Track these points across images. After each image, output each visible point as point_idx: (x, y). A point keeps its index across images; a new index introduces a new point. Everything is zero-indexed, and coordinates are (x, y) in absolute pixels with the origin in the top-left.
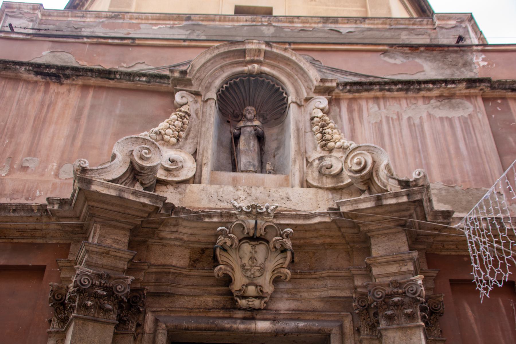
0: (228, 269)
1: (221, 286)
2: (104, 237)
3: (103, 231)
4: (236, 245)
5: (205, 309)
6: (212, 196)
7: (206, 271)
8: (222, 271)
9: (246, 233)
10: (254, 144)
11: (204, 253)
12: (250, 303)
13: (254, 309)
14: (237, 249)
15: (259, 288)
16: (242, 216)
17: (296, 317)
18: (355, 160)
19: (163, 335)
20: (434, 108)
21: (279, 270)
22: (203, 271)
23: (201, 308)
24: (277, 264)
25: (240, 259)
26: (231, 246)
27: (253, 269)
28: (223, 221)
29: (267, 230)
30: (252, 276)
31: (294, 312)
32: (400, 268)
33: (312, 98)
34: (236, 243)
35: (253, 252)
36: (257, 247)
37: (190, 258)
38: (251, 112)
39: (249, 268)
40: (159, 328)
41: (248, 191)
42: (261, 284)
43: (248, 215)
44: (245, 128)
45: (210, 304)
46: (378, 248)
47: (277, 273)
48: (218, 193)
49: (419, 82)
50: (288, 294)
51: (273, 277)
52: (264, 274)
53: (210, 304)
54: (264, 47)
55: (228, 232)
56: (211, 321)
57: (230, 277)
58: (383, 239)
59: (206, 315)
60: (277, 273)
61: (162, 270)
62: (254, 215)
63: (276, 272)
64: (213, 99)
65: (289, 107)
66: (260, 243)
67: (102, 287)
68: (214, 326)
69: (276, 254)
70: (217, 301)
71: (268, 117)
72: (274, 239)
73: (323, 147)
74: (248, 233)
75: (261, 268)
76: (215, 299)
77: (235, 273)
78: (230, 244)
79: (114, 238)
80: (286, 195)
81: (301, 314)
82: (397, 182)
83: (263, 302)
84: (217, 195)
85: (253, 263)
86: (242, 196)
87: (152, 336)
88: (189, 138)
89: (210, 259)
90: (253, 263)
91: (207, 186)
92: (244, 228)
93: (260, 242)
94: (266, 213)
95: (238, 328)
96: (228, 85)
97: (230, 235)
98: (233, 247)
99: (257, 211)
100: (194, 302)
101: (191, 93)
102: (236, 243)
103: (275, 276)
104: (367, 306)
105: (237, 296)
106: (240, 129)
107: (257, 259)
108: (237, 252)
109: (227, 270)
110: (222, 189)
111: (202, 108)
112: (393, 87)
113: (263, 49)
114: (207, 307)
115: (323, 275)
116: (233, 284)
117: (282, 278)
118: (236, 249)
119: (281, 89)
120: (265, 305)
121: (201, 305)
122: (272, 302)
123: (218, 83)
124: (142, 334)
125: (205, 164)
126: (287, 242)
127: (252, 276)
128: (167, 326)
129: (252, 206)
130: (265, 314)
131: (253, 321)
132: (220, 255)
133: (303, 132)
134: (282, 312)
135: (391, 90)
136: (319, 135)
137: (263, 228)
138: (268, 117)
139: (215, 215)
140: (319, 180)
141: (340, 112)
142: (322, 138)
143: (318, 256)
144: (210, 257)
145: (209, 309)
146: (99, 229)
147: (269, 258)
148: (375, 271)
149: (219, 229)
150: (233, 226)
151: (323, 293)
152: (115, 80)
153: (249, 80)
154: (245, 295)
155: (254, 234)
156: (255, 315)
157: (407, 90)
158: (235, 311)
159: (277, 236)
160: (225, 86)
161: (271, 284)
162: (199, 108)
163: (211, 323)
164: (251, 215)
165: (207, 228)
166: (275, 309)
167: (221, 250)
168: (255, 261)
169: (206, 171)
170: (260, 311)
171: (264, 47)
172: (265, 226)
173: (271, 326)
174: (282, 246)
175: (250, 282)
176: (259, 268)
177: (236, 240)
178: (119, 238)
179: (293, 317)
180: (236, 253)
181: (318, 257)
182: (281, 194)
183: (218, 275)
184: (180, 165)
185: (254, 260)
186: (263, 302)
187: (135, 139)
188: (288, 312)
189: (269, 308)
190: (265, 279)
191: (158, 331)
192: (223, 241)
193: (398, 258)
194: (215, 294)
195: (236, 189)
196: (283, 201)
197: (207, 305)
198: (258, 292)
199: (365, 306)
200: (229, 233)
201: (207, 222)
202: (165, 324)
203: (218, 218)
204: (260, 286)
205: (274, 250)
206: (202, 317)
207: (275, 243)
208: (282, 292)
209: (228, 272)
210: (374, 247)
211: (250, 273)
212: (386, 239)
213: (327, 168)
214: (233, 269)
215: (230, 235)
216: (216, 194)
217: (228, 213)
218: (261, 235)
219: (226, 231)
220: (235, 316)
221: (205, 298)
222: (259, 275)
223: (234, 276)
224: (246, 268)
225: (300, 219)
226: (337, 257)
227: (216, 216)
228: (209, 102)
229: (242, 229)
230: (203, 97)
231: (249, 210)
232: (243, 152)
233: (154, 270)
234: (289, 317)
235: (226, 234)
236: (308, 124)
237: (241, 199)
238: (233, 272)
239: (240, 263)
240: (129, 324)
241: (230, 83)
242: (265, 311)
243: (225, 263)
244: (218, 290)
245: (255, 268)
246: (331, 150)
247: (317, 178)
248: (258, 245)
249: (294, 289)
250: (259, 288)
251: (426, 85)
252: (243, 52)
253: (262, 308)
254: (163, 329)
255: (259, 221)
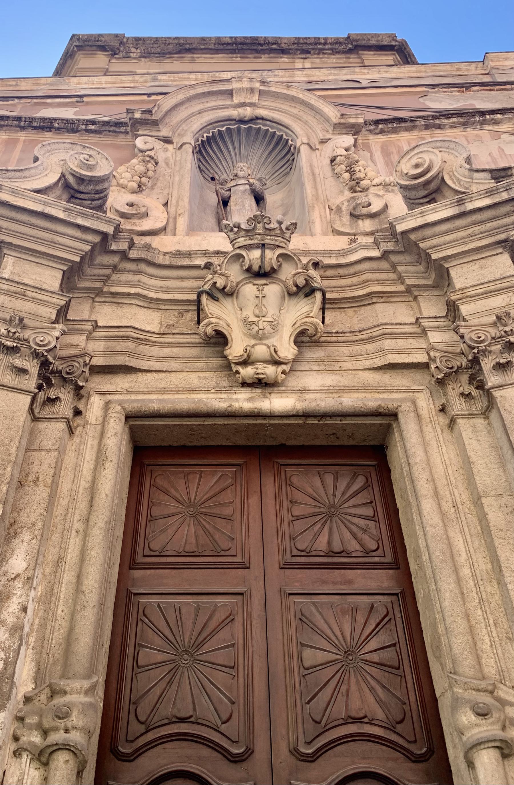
2: (20, 276)
3: (17, 268)
10: (251, 205)
18: (414, 161)
19: (117, 421)
20: (507, 143)
24: (299, 313)
32: (509, 299)
33: (330, 139)
37: (160, 323)
38: (244, 168)
40: (110, 411)
44: (237, 187)
45: (194, 382)
46: (466, 281)
49: (482, 113)
54: (257, 85)
58: (472, 268)
61: (116, 333)
64: (190, 144)
65: (299, 152)
67: (10, 337)
70: (205, 378)
71: (267, 182)
73: (353, 190)
76: (202, 376)
77: (232, 331)
79: (36, 279)
82: (487, 175)
87: (99, 427)
88: (156, 187)
89: (192, 324)
96: (211, 135)
100: (168, 380)
101: (159, 139)
104: (456, 368)
106: (230, 190)
111: (174, 156)
112: (445, 121)
113: (257, 88)
115: (375, 334)
117: (309, 332)
119: (284, 137)
123: (197, 124)
124: (84, 426)
125: (180, 215)
128: (124, 409)
133: (322, 177)
135: (442, 126)
136: (347, 176)
138: (267, 182)
140: (351, 225)
141: (371, 156)
142: (351, 178)
143: (361, 315)
144: (193, 321)
146: (11, 264)
148: (465, 309)
151: (376, 361)
152: (53, 130)
153: (239, 129)
155: (260, 267)
157: (465, 125)
160: (205, 135)
161: (292, 344)
162: (170, 156)
168: (264, 309)
169: (182, 223)
171: (257, 85)
178: (44, 280)
181: (362, 316)
184: (143, 210)
185: (263, 307)
187: (71, 146)
191: (108, 416)
193: (503, 285)
199: (452, 368)
202: (120, 404)
207: (295, 278)
209: (221, 329)
210: (457, 281)
212: (477, 266)
213: (363, 207)
226: (394, 313)
228: (184, 147)
230: (175, 144)
232: (236, 212)
233: (103, 334)
234: (42, 668)
236: (328, 168)
238: (229, 329)
240: (60, 406)
241: (213, 132)
246: (365, 190)
247: (348, 223)
248: (267, 284)
251: (492, 116)
252: (230, 93)
254: (117, 412)
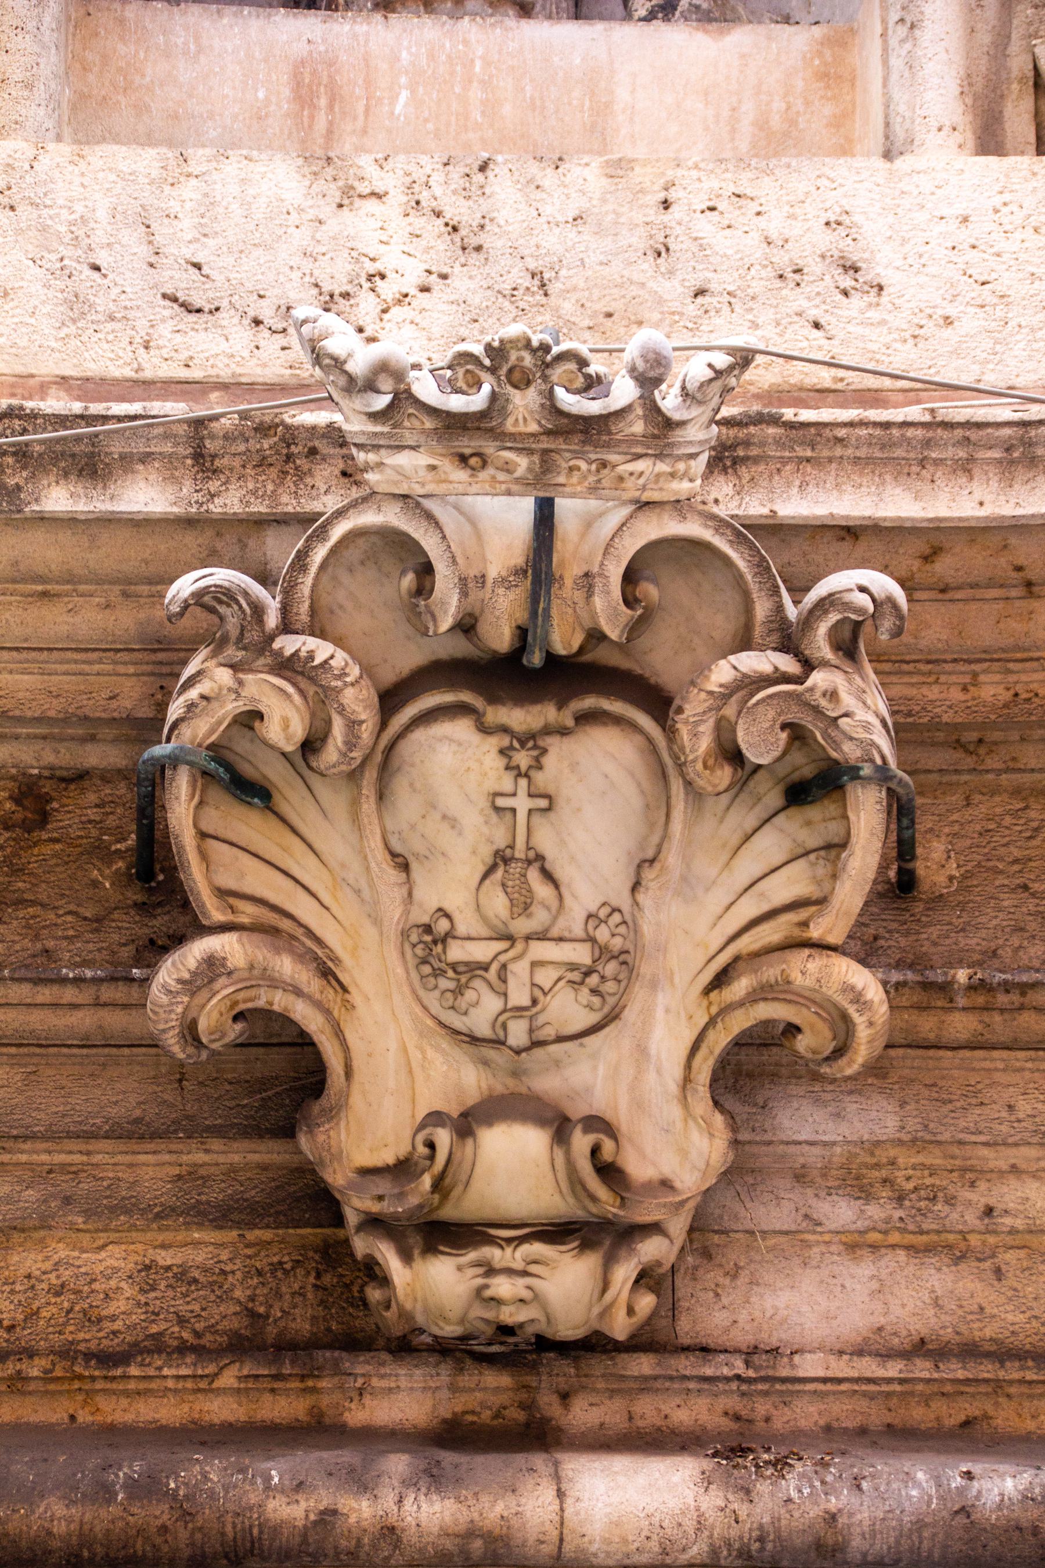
0: (286, 966)
1: (218, 1132)
4: (351, 745)
5: (67, 1353)
6: (102, 258)
7: (69, 994)
8: (224, 989)
9: (446, 623)
11: (43, 818)
12: (503, 1287)
13: (544, 1344)
14: (370, 775)
15: (581, 1142)
16: (403, 459)
17: (953, 1414)
21: (771, 973)
22: (46, 994)
23: (31, 1354)
24: (749, 909)
25: (394, 875)
26: (310, 746)
27: (520, 970)
28: (216, 508)
29: (649, 590)
30: (518, 1033)
31: (922, 1369)
34: (353, 725)
35: (522, 804)
36: (558, 751)
39: (482, 952)
41: (456, 209)
42: (599, 1103)
43: (467, 444)
45: (118, 1306)
47: (756, 996)
48: (162, 231)
50: (864, 1192)
51: (720, 1040)
52: (630, 1015)
53: (118, 1306)
55: (272, 620)
56: (132, 1468)
57: (304, 1042)
59: (84, 1417)
60: (756, 996)
62: (520, 443)
63: (741, 986)
66: (585, 718)
68: (161, 1513)
69: (742, 818)
70: (182, 1276)
72: (722, 673)
74: (467, 626)
75: (603, 953)
76: (165, 1258)
77: (349, 1006)
78: (299, 731)
80: (825, 240)
81: (998, 1385)
83: (624, 1273)
84: (144, 251)
85: (524, 905)
86: (390, 259)
90: (524, 905)
91: (45, 162)
92: (426, 570)
93: (589, 702)
94: (638, 427)
95: (390, 1532)
97: (289, 644)
98: (330, 755)
99: (553, 409)
102: (353, 725)
103: (739, 1022)
105: (374, 1223)
107: (563, 871)
108: (368, 806)
109: (274, 983)
110: (190, 190)
114: (89, 1338)
116: (332, 1114)
117: (803, 1043)
118: (354, 776)
120: (646, 1302)
121: (33, 1315)
122: (713, 1276)
126: (848, 701)
127: (518, 1033)
129: (497, 352)
130: (646, 1385)
131: (539, 1460)
132: (203, 835)
134: (810, 1366)
137: (615, 572)
139: (140, 447)
145: (108, 1359)
147: (672, 858)
149: (185, 586)
150: (320, 553)
154: (449, 1212)
156: (548, 1403)
158: (361, 1366)
159: (744, 643)
161: (701, 1100)
163: (133, 1488)
164: (490, 448)
165: (71, 579)
166: (741, 1338)
167: (216, 794)
168: (542, 890)
170: (597, 1365)
172: (630, 546)
173: (712, 1501)
174: (797, 734)
175: (501, 1085)
176: (582, 954)
177: (349, 696)
179: (918, 1415)
180: (355, 818)
182: (775, 224)
183: (190, 1032)
186: (624, 1273)
188: (869, 1367)
189: (686, 1329)
190: (642, 1051)
192: (231, 707)
194: (162, 1215)
195: (334, 194)
196: (797, 300)
197: (95, 1321)
198: (575, 1182)
200: (287, 627)
201: (70, 522)
203: (172, 479)
204: (596, 1123)
205: (725, 775)
206: (44, 1432)
208: (800, 1177)
209: (280, 1001)
211: (491, 1004)
214: (326, 973)
215: (289, 644)
216: (132, 239)
217: (263, 429)
218: (595, 636)
219: (258, 610)
220: (357, 1416)
221: (63, 1252)
222: (584, 1019)
223: (339, 1034)
224: (456, 952)
225: (966, 467)
227: (145, 458)
229: (408, 580)
231: (476, 401)
234: (877, 1416)
235: (253, 636)
237: (388, 289)
239: (393, 912)
242: (643, 1365)
243: (248, 912)
244: (191, 1176)
245: (540, 950)
249: (915, 1143)
250: (581, 1142)
253: (620, 1328)
255: (567, 509)
